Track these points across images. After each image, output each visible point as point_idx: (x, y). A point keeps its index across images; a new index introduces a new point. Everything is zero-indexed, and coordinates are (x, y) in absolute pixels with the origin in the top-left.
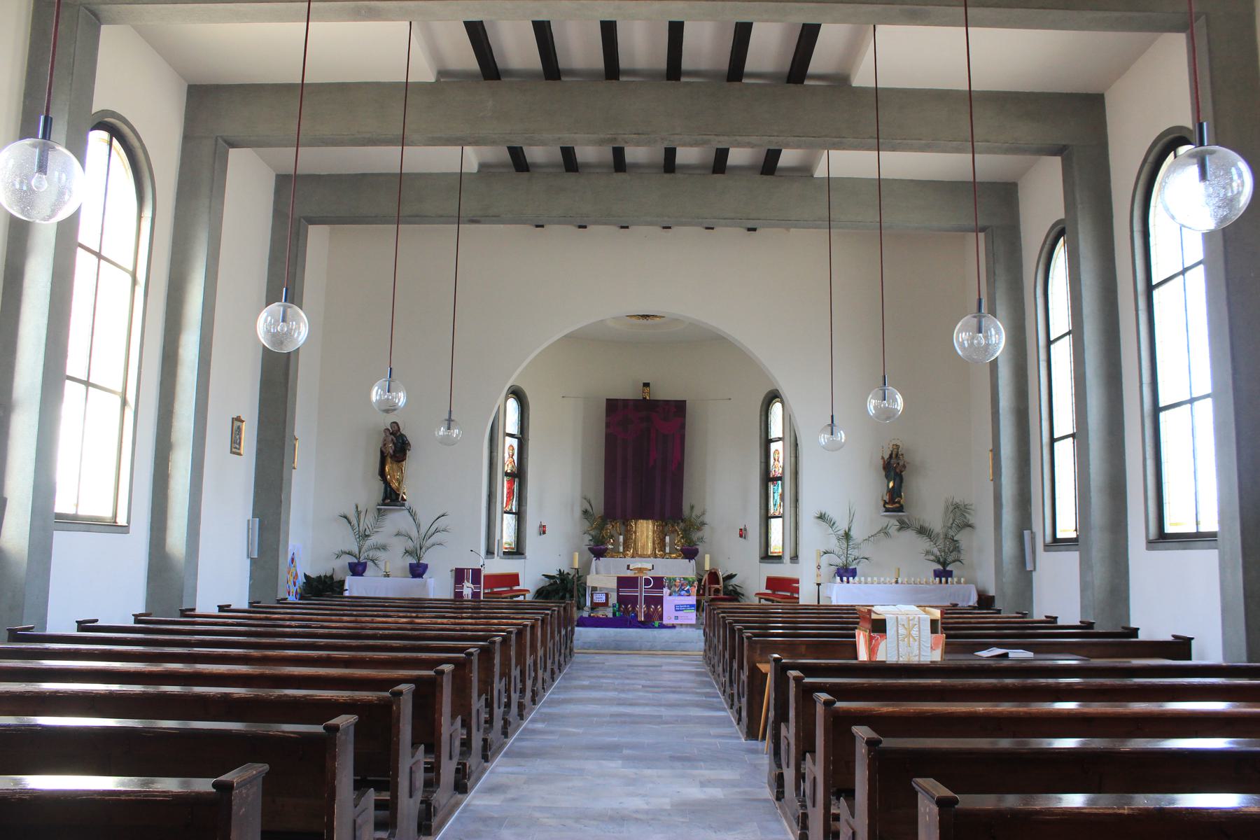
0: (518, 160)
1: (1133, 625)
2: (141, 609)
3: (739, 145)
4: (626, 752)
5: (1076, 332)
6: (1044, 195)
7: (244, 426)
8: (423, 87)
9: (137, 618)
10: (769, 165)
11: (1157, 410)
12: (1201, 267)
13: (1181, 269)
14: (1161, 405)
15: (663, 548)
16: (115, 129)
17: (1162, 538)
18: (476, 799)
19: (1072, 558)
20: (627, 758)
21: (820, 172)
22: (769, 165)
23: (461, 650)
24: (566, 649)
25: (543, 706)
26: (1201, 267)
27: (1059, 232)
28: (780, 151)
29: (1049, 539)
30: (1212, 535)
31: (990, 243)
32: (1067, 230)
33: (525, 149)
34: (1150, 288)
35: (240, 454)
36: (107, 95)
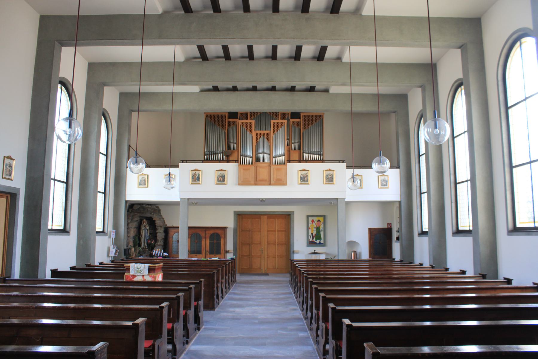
0: (204, 56)
1: (448, 267)
2: (74, 264)
3: (308, 44)
4: (257, 321)
5: (470, 131)
6: (451, 68)
7: (14, 163)
8: (180, 63)
9: (72, 268)
10: (320, 56)
11: (511, 167)
12: (466, 133)
13: (524, 98)
14: (514, 165)
15: (384, 180)
16: (64, 83)
17: (515, 230)
18: (192, 347)
19: (468, 240)
20: (257, 319)
21: (346, 59)
22: (320, 56)
23: (211, 271)
24: (234, 281)
25: (226, 300)
26: (466, 133)
27: (458, 85)
28: (327, 47)
29: (511, 226)
30: (470, 231)
31: (424, 91)
32: (464, 83)
33: (205, 46)
34: (507, 108)
35: (11, 180)
36: (65, 72)
